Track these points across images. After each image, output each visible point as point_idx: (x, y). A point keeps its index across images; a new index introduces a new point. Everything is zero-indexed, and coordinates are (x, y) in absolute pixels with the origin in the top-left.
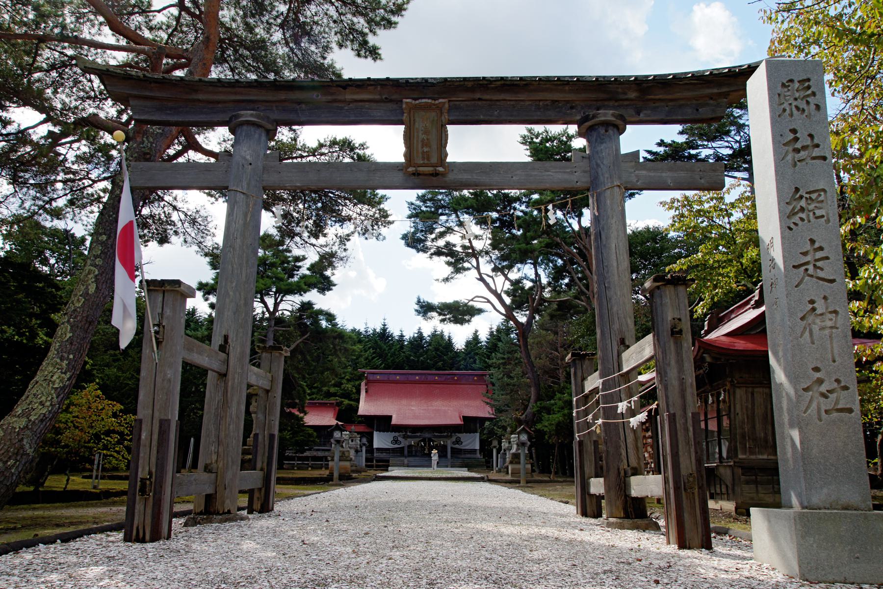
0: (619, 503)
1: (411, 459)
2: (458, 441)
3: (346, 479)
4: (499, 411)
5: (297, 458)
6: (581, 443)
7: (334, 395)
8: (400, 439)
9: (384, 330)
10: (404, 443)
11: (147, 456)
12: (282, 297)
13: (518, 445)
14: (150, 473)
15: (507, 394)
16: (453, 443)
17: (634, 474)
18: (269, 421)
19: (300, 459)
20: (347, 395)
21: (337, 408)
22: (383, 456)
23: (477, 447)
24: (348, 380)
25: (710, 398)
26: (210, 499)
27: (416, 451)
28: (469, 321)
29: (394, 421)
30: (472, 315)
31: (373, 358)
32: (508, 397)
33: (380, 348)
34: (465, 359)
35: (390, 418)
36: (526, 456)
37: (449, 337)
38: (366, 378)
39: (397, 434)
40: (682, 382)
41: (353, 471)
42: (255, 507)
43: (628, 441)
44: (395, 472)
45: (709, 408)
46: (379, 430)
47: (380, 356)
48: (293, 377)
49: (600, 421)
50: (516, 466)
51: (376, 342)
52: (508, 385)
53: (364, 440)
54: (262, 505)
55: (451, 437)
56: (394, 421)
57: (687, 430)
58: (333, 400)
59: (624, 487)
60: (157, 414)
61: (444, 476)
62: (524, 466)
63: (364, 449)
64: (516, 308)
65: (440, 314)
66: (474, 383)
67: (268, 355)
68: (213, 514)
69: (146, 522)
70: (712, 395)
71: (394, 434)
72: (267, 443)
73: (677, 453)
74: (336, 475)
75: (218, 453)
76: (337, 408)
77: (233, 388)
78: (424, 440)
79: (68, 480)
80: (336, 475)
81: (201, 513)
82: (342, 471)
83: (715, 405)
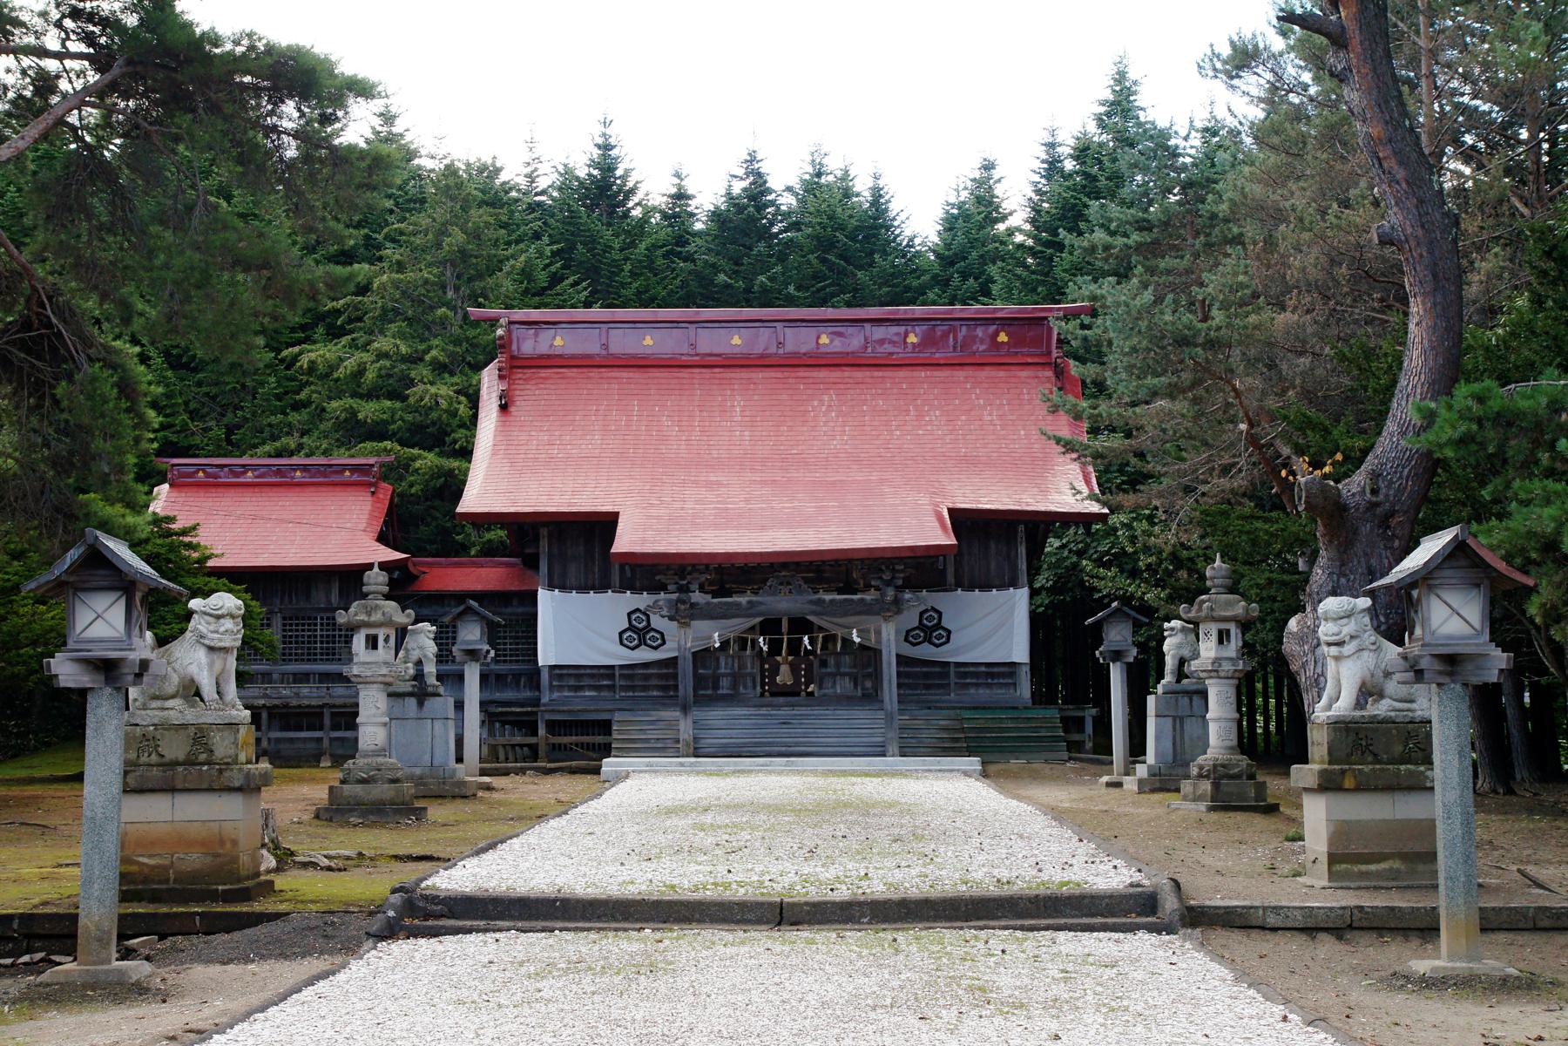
7: (377, 432)
8: (657, 622)
9: (606, 164)
15: (1173, 392)
16: (907, 637)
21: (386, 490)
22: (584, 703)
23: (1020, 652)
24: (440, 368)
29: (625, 541)
32: (1181, 405)
35: (606, 524)
37: (877, 193)
39: (643, 600)
46: (559, 583)
51: (574, 215)
52: (1183, 342)
55: (897, 606)
56: (625, 541)
58: (368, 455)
61: (877, 888)
66: (996, 360)
76: (386, 490)
79: (225, 650)
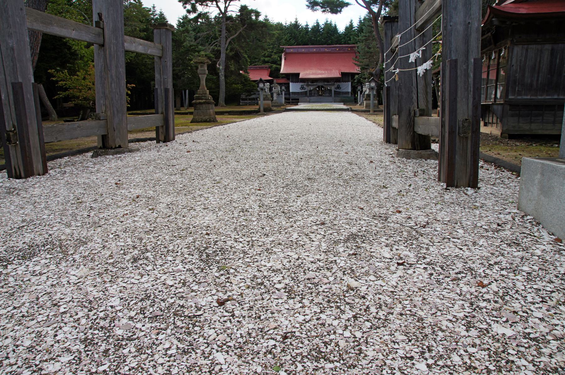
0: (409, 138)
1: (312, 98)
2: (339, 87)
3: (268, 111)
4: (363, 69)
5: (241, 99)
6: (388, 88)
7: (268, 62)
10: (307, 89)
11: (9, 113)
12: (230, 3)
13: (369, 89)
14: (14, 126)
15: (367, 58)
17: (421, 115)
18: (164, 79)
19: (250, 99)
20: (274, 62)
21: (269, 70)
22: (296, 97)
23: (350, 90)
25: (494, 55)
26: (104, 138)
27: (314, 94)
28: (340, 11)
29: (301, 76)
30: (342, 7)
31: (290, 39)
32: (368, 60)
33: (294, 33)
34: (344, 38)
36: (374, 96)
37: (335, 25)
38: (285, 51)
39: (303, 84)
40: (467, 25)
41: (273, 106)
42: (160, 138)
43: (419, 87)
44: (301, 106)
45: (491, 63)
46: (292, 82)
47: (295, 38)
48: (240, 52)
49: (398, 70)
50: (368, 102)
52: (368, 52)
53: (283, 88)
54: (165, 138)
57: (467, 76)
58: (267, 65)
59: (411, 124)
60: (8, 78)
62: (373, 101)
63: (283, 93)
64: (373, 3)
65: (322, 7)
67: (159, 31)
68: (109, 148)
69: (19, 163)
70: (495, 52)
71: (301, 84)
72: (163, 94)
73: (455, 99)
74: (262, 109)
75: (105, 105)
76: (269, 70)
77: (110, 55)
78: (318, 87)
80: (262, 109)
81: (101, 148)
82: (266, 106)
83: (496, 60)
